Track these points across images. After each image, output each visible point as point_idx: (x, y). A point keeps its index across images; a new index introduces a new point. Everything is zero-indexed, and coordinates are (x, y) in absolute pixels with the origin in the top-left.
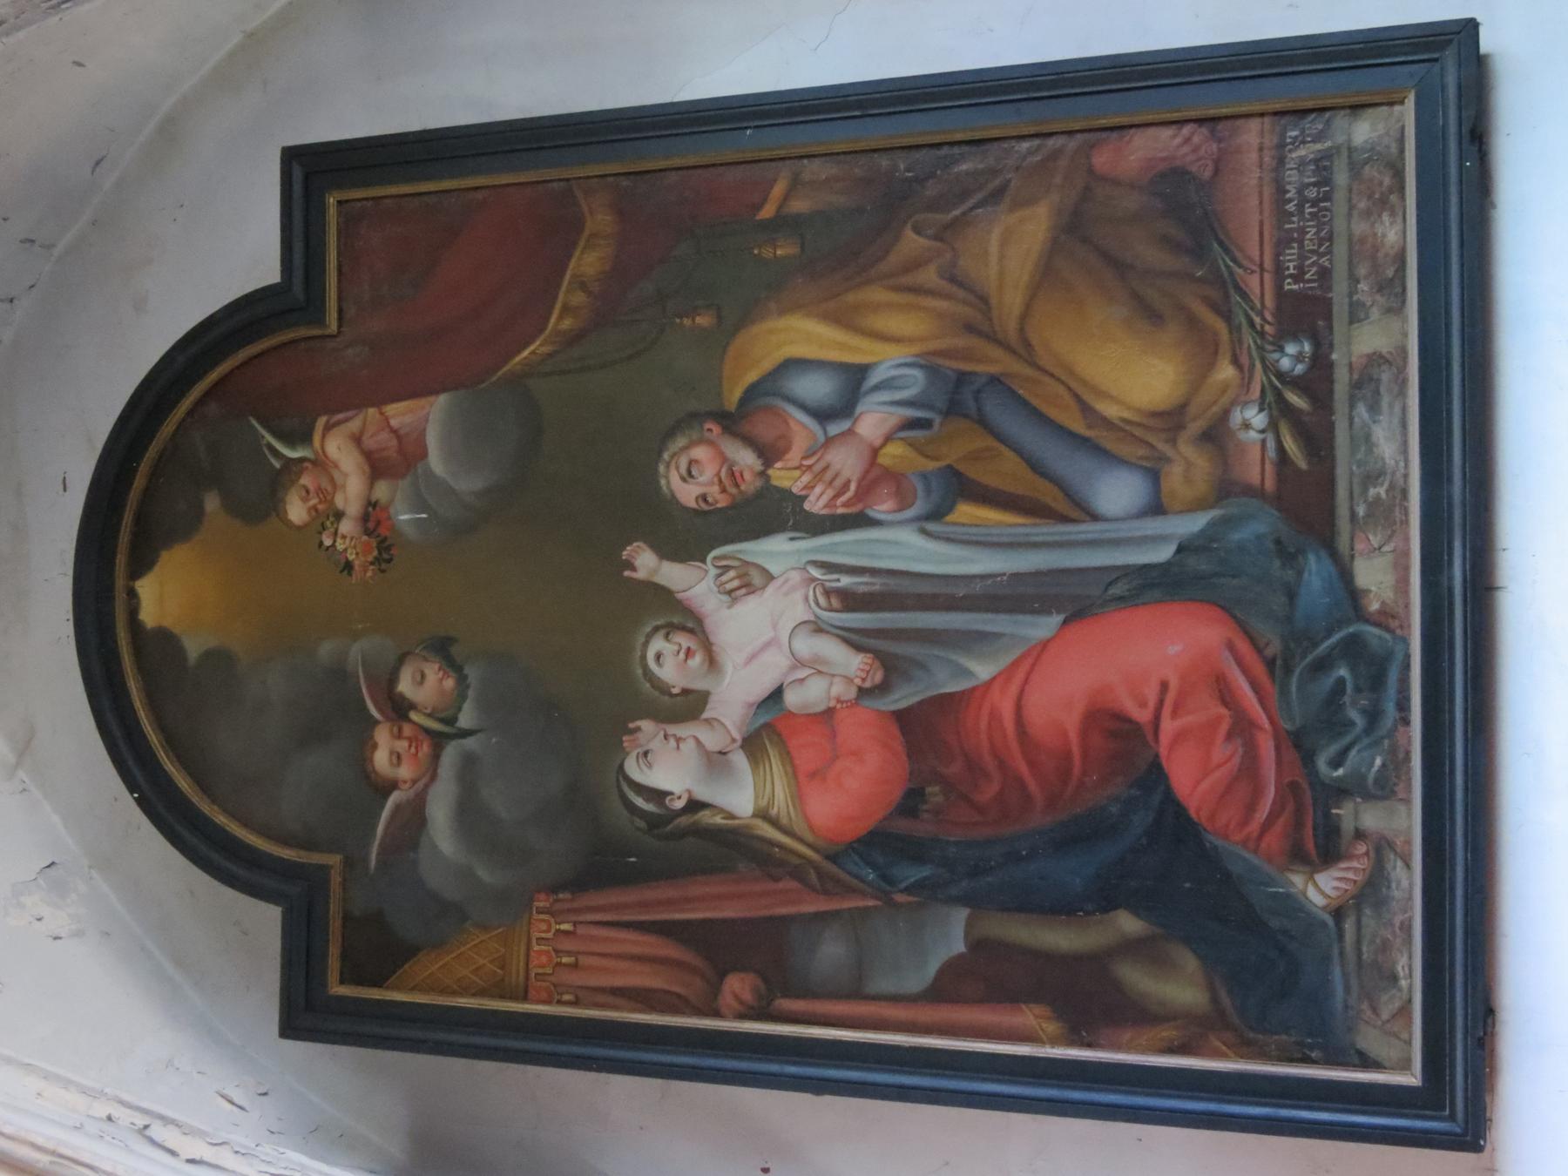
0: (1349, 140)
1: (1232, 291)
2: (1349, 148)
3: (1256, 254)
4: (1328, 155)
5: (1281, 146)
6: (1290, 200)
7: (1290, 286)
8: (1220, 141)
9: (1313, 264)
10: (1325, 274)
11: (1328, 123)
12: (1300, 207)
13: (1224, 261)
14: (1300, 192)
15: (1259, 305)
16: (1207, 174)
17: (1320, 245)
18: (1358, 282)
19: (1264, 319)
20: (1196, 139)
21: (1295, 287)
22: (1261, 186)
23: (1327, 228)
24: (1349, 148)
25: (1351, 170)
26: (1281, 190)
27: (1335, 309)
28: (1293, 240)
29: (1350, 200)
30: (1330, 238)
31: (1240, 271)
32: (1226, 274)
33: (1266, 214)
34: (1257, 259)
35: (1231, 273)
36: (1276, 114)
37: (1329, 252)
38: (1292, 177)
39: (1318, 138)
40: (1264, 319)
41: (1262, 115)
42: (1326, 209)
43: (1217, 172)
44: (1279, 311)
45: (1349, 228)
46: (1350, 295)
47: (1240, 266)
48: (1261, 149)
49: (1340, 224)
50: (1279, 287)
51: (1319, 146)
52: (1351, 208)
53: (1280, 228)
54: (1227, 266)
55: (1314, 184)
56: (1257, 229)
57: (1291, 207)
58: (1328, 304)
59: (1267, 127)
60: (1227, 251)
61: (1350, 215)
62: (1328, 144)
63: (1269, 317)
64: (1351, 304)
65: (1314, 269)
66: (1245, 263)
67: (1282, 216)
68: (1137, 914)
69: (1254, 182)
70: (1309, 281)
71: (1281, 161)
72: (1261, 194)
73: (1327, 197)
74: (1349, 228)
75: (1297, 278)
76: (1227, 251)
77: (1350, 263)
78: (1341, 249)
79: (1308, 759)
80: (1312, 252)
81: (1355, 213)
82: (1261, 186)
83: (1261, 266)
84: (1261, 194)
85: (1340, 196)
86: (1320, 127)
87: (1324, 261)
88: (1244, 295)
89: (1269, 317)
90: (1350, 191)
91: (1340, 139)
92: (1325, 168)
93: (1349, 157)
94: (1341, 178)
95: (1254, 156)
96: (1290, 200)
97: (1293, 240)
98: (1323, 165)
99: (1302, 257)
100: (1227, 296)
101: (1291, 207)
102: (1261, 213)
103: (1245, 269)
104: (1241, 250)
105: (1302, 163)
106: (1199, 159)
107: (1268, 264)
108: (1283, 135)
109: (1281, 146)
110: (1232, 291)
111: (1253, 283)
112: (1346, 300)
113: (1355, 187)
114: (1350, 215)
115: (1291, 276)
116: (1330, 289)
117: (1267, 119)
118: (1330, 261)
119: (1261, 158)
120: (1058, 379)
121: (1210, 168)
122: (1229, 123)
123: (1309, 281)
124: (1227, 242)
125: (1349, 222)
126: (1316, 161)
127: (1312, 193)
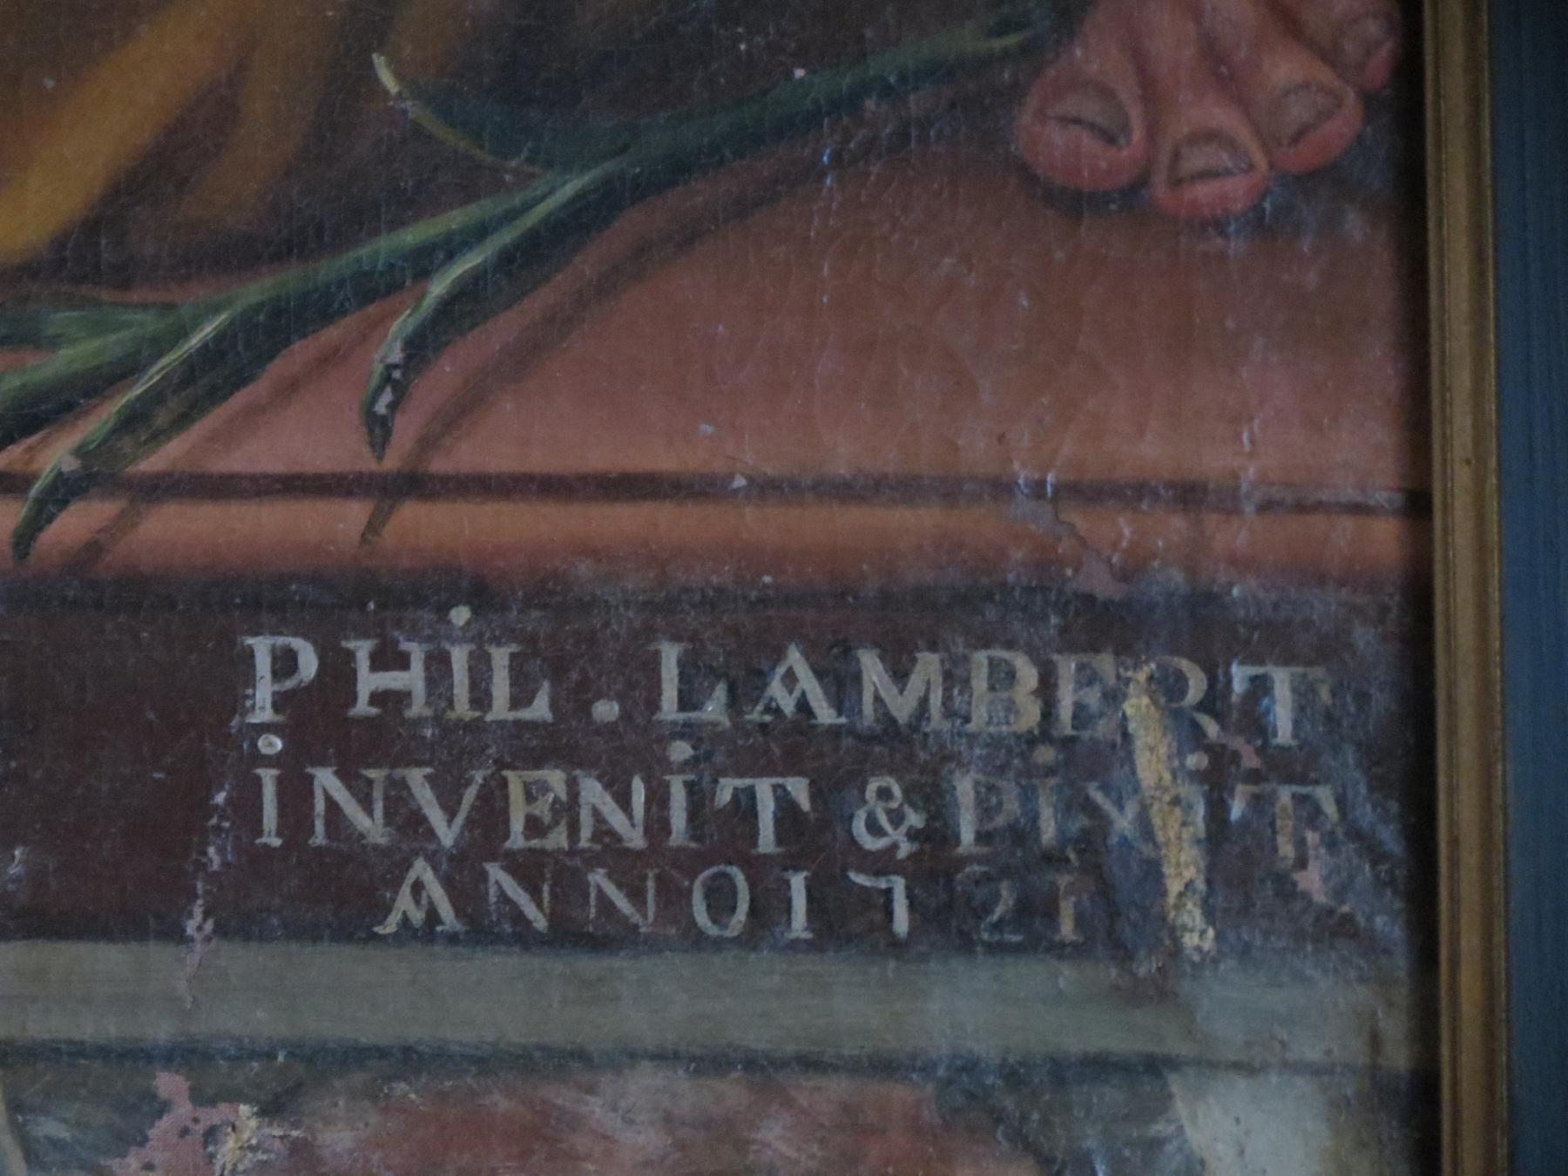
0: (1209, 1065)
1: (255, 290)
2: (1156, 1066)
3: (484, 449)
4: (1118, 917)
5: (1205, 626)
6: (842, 685)
7: (272, 668)
8: (1264, 225)
9: (409, 823)
10: (335, 896)
11: (1335, 929)
12: (793, 744)
13: (457, 241)
14: (894, 741)
15: (153, 463)
16: (1053, 138)
17: (527, 869)
18: (270, 1110)
19: (64, 491)
20: (1285, 69)
21: (262, 708)
22: (950, 490)
23: (645, 918)
24: (1156, 1066)
25: (1014, 1076)
26: (910, 617)
27: (107, 959)
28: (575, 702)
29: (811, 1064)
30: (574, 934)
31: (402, 324)
32: (383, 247)
33: (760, 524)
34: (469, 454)
35: (377, 287)
36: (1421, 590)
37: (484, 928)
38: (1002, 693)
39: (1238, 864)
40: (64, 491)
41: (1418, 505)
42: (768, 909)
43: (1074, 203)
44: (138, 593)
45: (628, 1056)
46: (187, 1056)
47: (420, 348)
48: (1188, 495)
49: (654, 997)
50: (266, 594)
51: (1184, 867)
52: (760, 1068)
53: (663, 610)
54: (424, 262)
55: (936, 836)
56: (664, 459)
57: (795, 683)
58: (145, 918)
59: (1341, 537)
60: (531, 257)
61: (710, 1062)
62: (1197, 936)
63: (75, 524)
64: (138, 1056)
65: (370, 826)
66: (447, 373)
67: (742, 626)
68: (143, 474)
69: (976, 451)
70: (296, 793)
71: (1106, 625)
72: (906, 489)
73: (845, 922)
74: (628, 1056)
75: (319, 719)
76: (531, 257)
77: (409, 1059)
78: (490, 1000)
79: (682, 736)
80: (490, 817)
81: (731, 1092)
82: (950, 490)
83: (413, 484)
84: (906, 489)
85: (850, 1003)
86: (1312, 881)
87: (423, 891)
88: (217, 374)
89: (75, 524)
90: (885, 1067)
91: (1229, 1003)
92: (1035, 912)
93: (1099, 1066)
94: (970, 1009)
95: (1150, 452)
96: (842, 685)
97: (575, 702)
98: (1048, 888)
99: (456, 749)
100: (236, 255)
101: (795, 683)
102: (765, 489)
103: (399, 382)
104: (524, 359)
105: (1090, 760)
106: (1152, 94)
107: (426, 526)
108: (1275, 638)
109: (1205, 626)
110: (255, 290)
111: (307, 430)
112: (161, 1031)
113: (900, 1094)
114: (710, 1062)
115: (338, 671)
116: (236, 925)
117: (1385, 538)
118: (429, 930)
119: (1131, 493)
120: (1506, 877)
121: (1098, 163)
122: (1379, 293)
123: (296, 793)
124: (587, 263)
125: (664, 1057)
126: (1090, 844)
127: (881, 820)
